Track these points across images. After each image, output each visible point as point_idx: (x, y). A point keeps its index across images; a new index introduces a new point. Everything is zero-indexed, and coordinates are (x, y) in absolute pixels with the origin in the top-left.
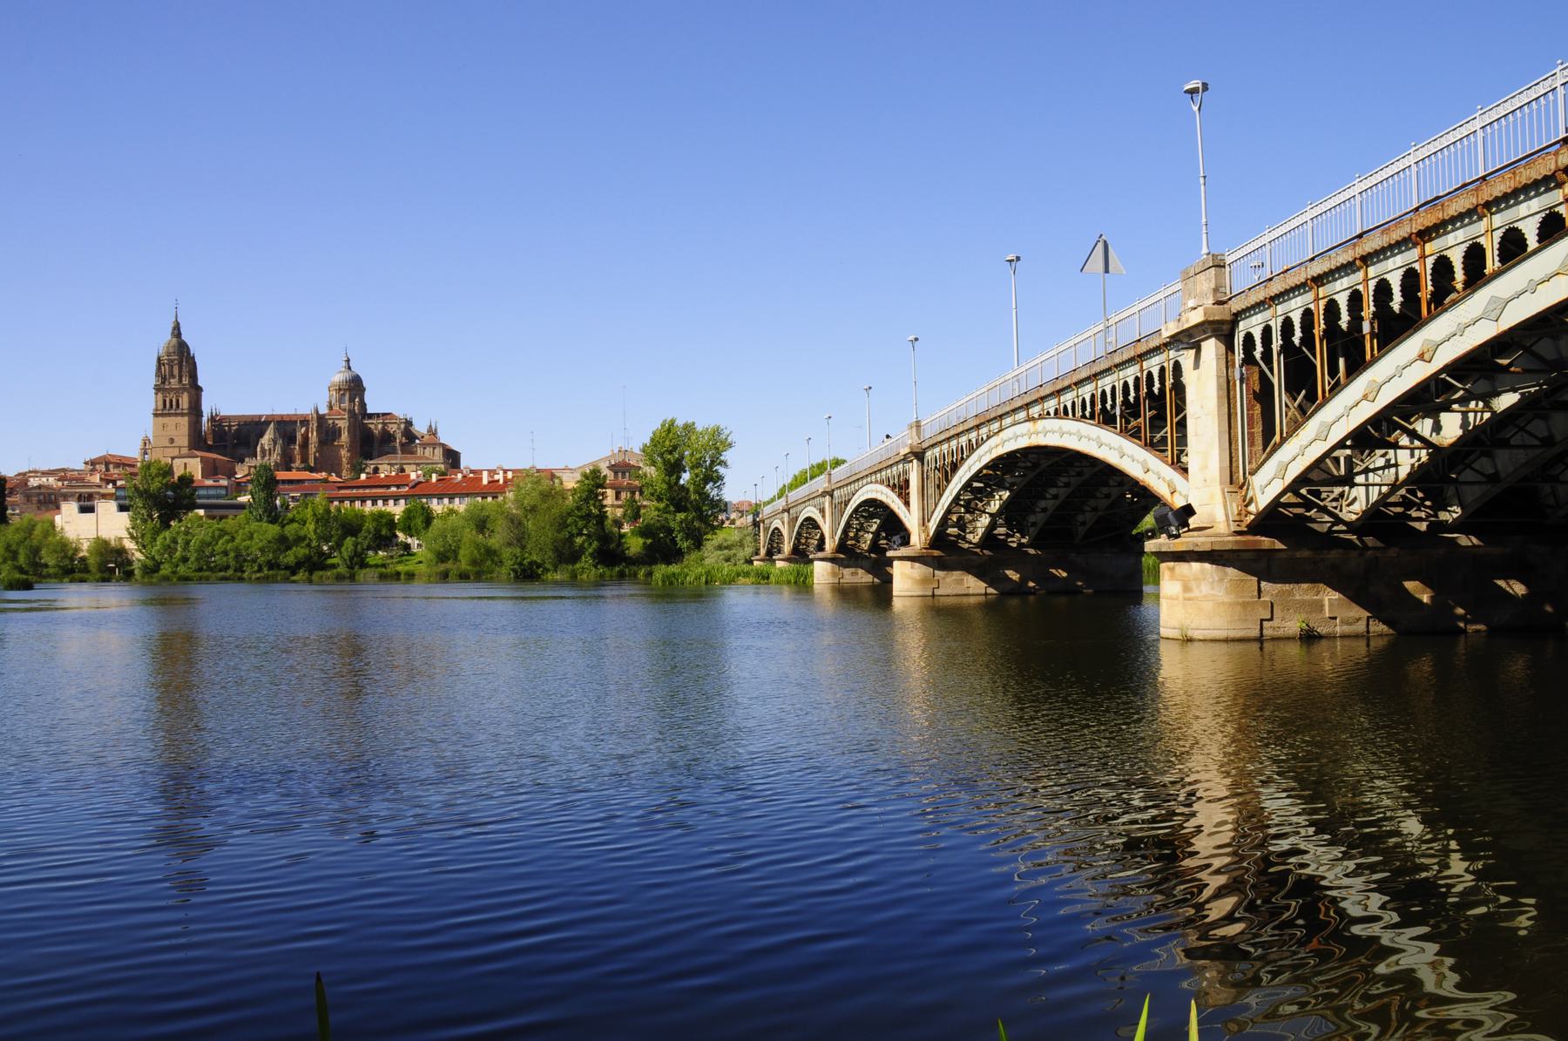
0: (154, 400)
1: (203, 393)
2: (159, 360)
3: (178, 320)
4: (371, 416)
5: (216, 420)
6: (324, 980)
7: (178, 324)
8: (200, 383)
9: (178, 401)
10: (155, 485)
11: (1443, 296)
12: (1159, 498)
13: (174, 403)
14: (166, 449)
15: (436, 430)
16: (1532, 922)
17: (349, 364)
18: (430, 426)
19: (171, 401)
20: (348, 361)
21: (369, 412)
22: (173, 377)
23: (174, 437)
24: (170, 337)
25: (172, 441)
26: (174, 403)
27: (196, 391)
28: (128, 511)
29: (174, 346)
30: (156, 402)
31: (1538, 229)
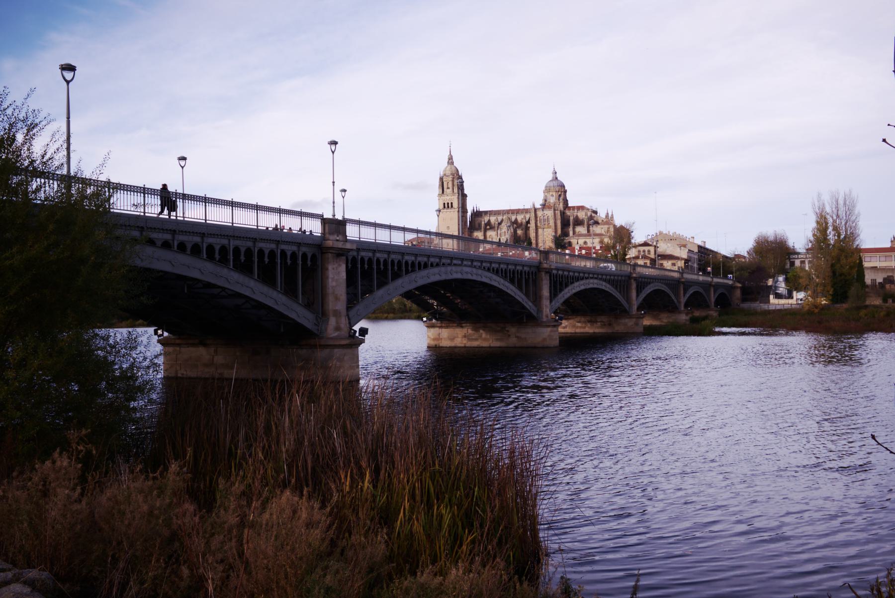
2: (441, 179)
8: (466, 192)
9: (452, 203)
13: (450, 205)
15: (612, 215)
18: (608, 214)
19: (448, 203)
21: (570, 205)
22: (448, 188)
26: (450, 205)
27: (463, 197)
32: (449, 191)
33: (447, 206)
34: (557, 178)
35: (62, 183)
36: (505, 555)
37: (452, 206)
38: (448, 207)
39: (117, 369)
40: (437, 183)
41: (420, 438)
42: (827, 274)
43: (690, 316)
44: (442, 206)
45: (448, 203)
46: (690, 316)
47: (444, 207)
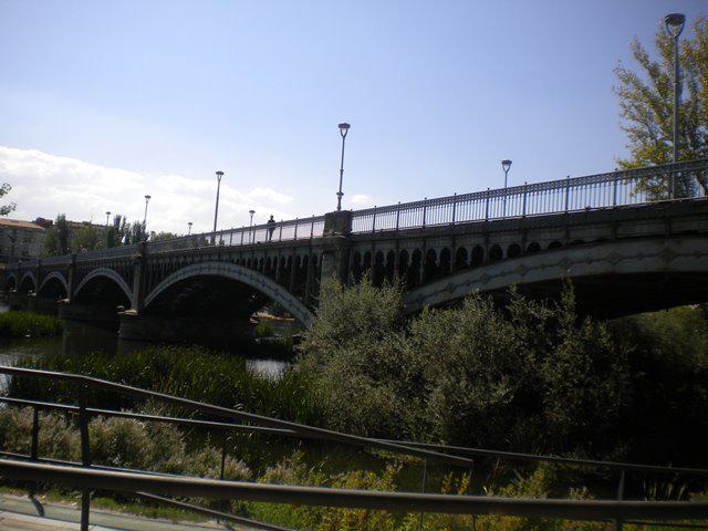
11: (461, 266)
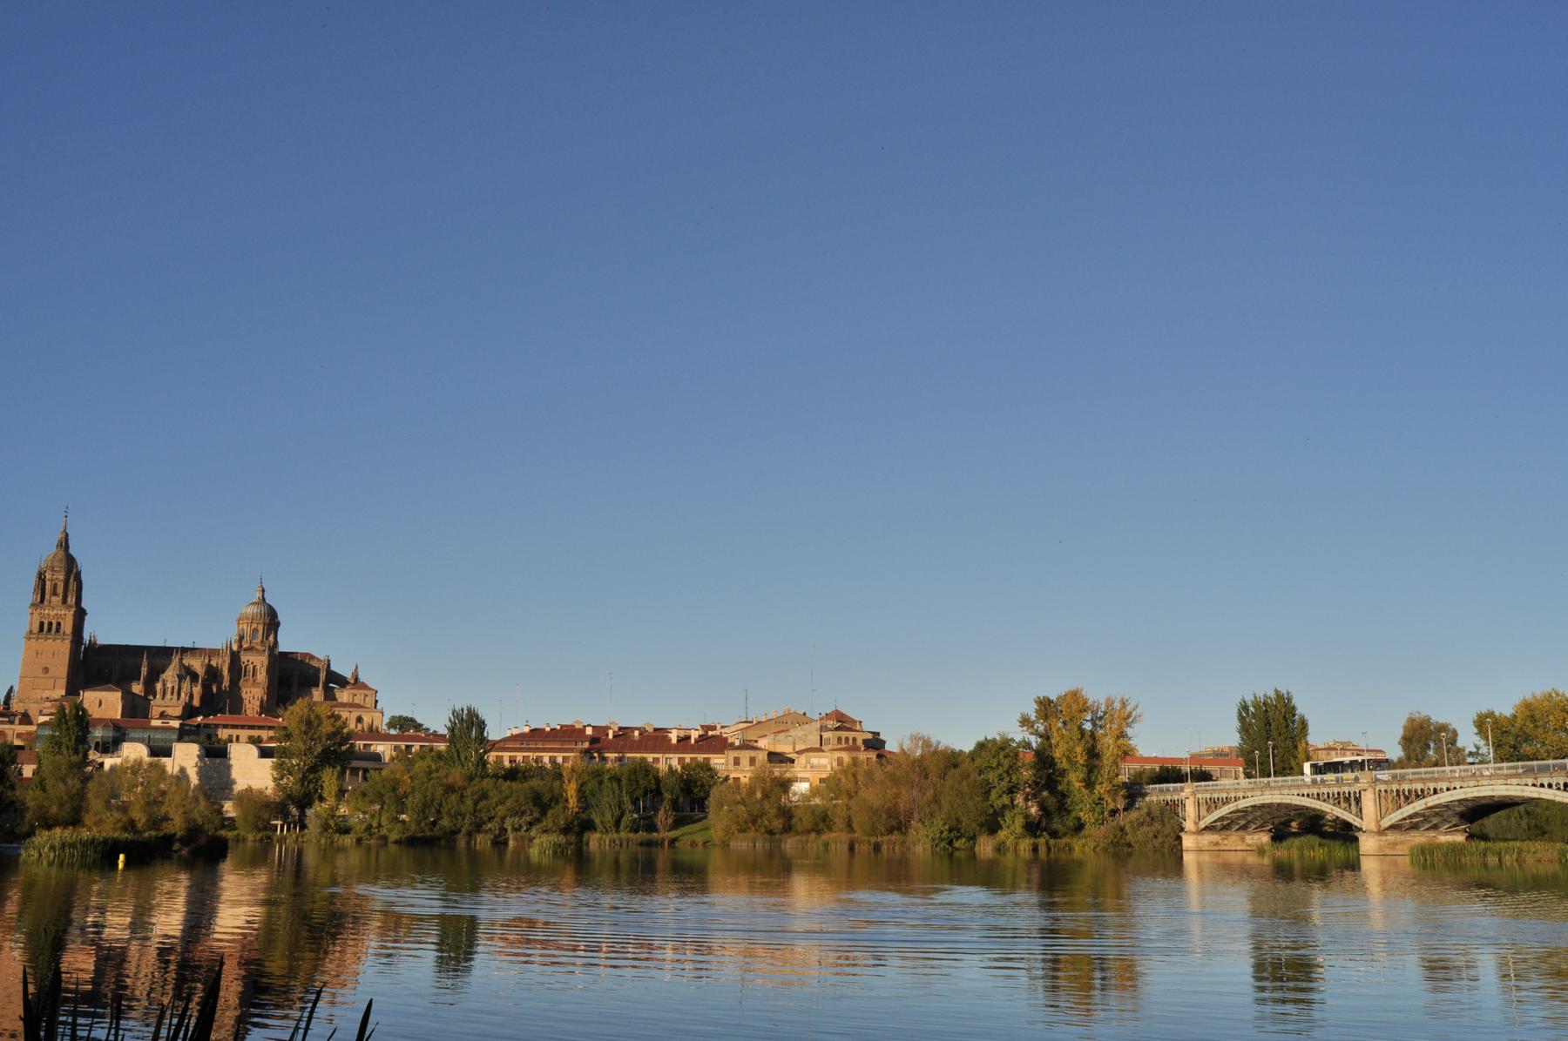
0: (28, 621)
1: (86, 617)
3: (67, 531)
4: (494, 746)
5: (92, 645)
6: (502, 846)
7: (67, 535)
8: (84, 605)
9: (59, 624)
10: (983, 819)
12: (1182, 871)
14: (37, 680)
16: (549, 766)
17: (263, 595)
19: (50, 624)
20: (263, 591)
22: (55, 593)
23: (48, 666)
24: (54, 549)
25: (46, 670)
27: (80, 615)
28: (272, 757)
29: (60, 560)
30: (31, 624)
31: (884, 742)
32: (57, 600)
33: (46, 629)
34: (264, 599)
35: (403, 755)
36: (701, 962)
37: (58, 630)
38: (50, 630)
39: (118, 884)
40: (32, 581)
41: (852, 829)
42: (807, 882)
43: (902, 813)
44: (36, 628)
45: (50, 624)
46: (902, 813)
47: (41, 629)
